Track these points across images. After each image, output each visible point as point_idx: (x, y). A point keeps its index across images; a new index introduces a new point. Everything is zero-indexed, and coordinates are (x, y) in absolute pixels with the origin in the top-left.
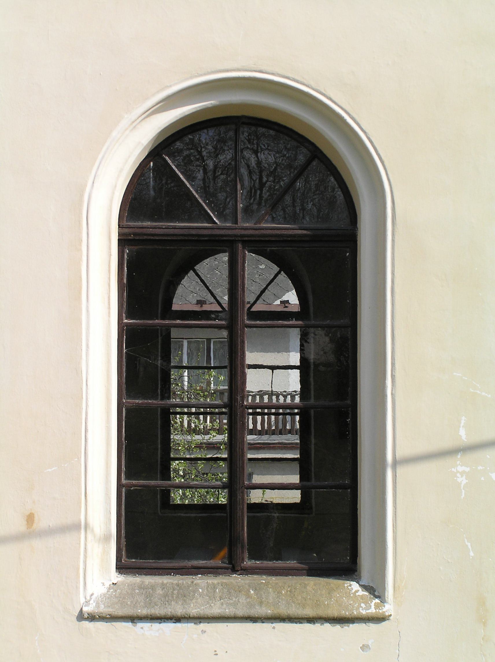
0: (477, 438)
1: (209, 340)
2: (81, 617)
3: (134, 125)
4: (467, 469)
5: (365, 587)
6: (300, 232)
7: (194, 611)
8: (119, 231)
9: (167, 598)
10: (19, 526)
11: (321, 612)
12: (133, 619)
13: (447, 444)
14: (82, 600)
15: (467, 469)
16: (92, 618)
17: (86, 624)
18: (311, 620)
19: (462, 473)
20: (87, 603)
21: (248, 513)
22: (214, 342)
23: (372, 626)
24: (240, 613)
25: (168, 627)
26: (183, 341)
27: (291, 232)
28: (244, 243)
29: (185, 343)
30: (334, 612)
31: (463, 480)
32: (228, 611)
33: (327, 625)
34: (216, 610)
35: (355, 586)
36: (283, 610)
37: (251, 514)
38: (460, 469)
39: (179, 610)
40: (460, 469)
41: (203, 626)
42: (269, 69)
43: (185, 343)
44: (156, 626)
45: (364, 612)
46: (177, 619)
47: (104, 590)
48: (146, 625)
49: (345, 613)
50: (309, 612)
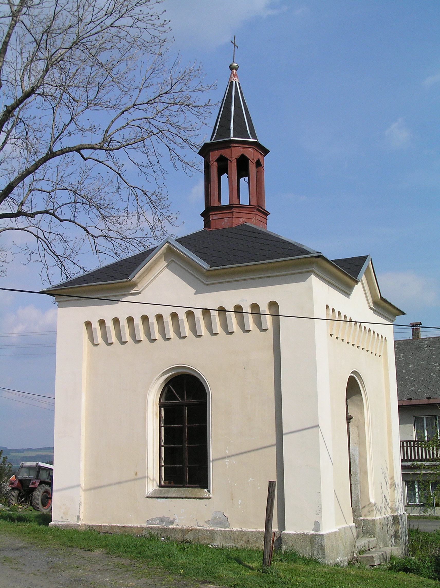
0: (231, 454)
1: (435, 416)
2: (146, 497)
3: (158, 379)
4: (228, 461)
5: (208, 491)
6: (197, 402)
7: (169, 496)
8: (160, 404)
9: (164, 493)
10: (133, 476)
11: (196, 496)
12: (157, 498)
13: (223, 455)
14: (147, 493)
15: (228, 461)
16: (148, 497)
17: (147, 499)
18: (194, 498)
19: (227, 462)
20: (148, 494)
21: (52, 454)
22: (438, 417)
23: (207, 500)
24: (179, 496)
25: (164, 499)
26: (423, 417)
27: (195, 402)
28: (185, 405)
29: (425, 418)
30: (199, 497)
31: (227, 463)
32: (176, 496)
33: (198, 500)
34: (174, 496)
35: (206, 490)
36: (188, 496)
37: (52, 454)
38: (227, 460)
39: (166, 496)
40: (227, 460)
41: (171, 499)
42: (185, 364)
43: (425, 418)
44: (162, 499)
45: (205, 496)
46: (166, 498)
47: (152, 491)
48: (160, 499)
49: (201, 497)
50: (193, 496)
